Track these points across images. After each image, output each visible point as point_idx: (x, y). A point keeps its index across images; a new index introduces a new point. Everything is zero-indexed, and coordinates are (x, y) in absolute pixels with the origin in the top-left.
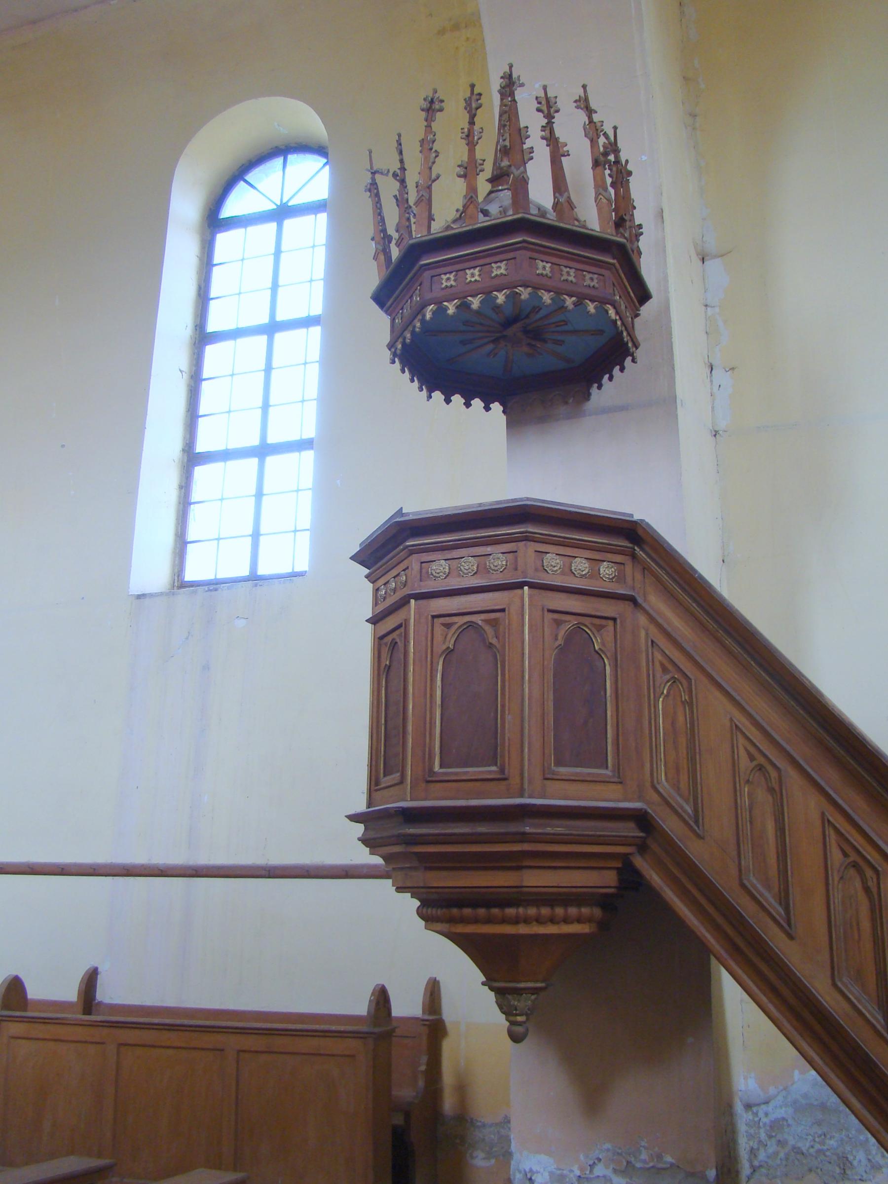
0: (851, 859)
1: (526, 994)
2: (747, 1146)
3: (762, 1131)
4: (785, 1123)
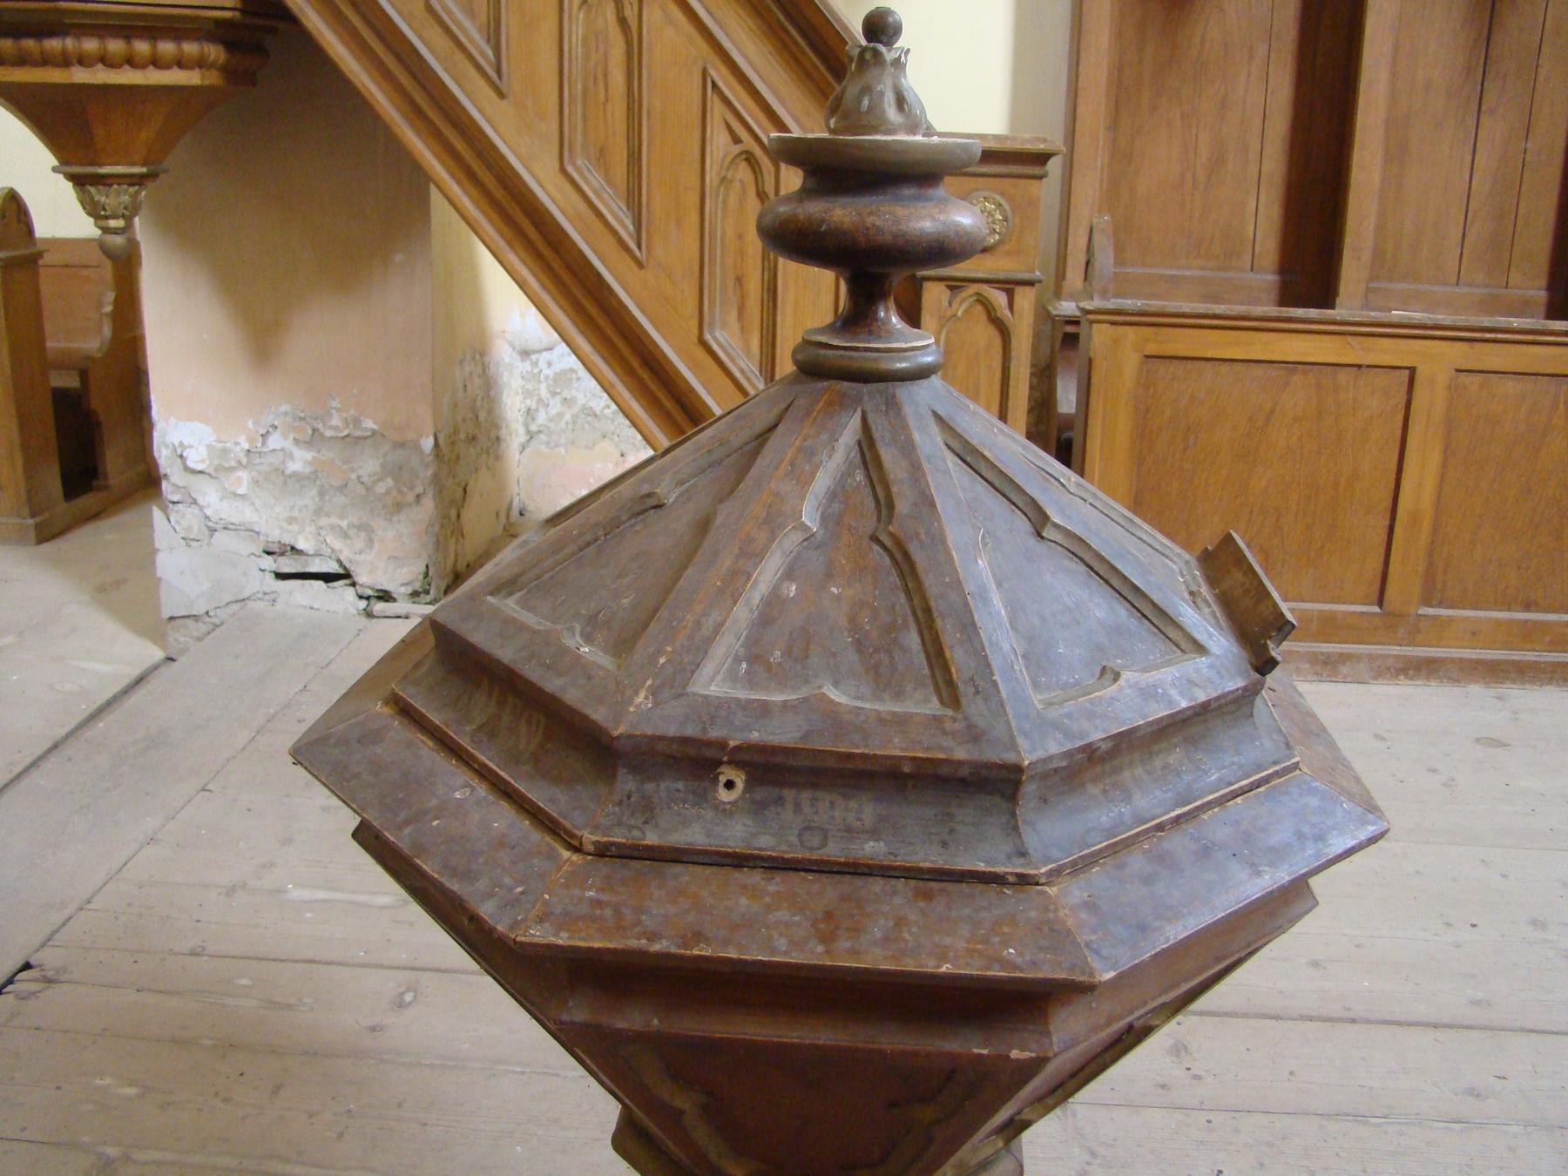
1: (119, 184)
2: (523, 405)
4: (574, 376)
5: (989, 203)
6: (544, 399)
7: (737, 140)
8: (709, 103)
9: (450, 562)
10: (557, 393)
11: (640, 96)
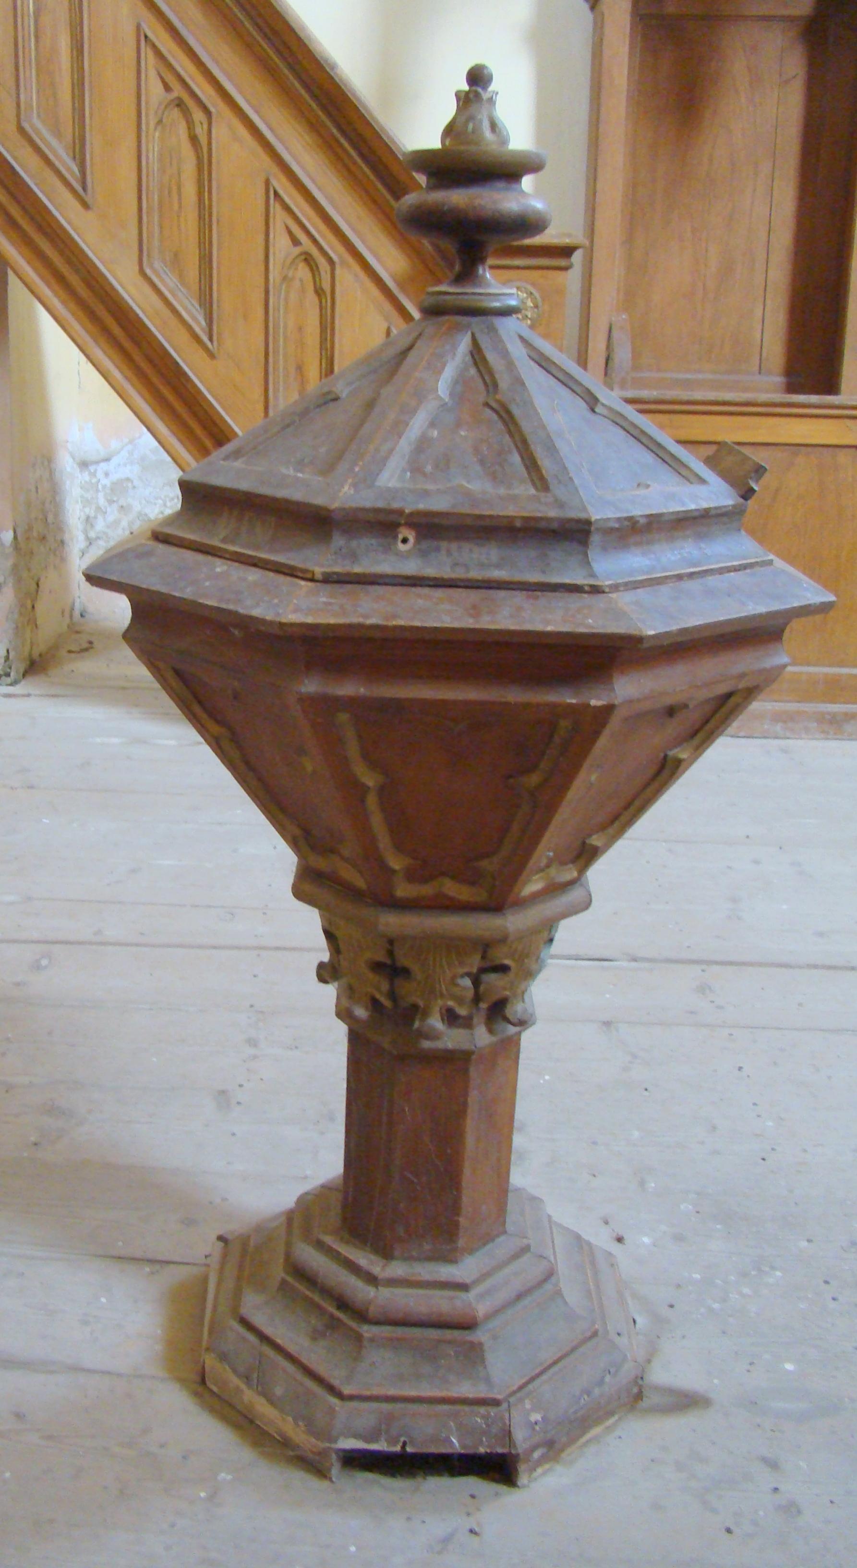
0: (175, 94)
2: (82, 514)
3: (101, 495)
4: (130, 485)
5: (521, 291)
6: (103, 508)
7: (296, 242)
8: (272, 209)
9: (26, 653)
10: (114, 501)
11: (210, 206)
